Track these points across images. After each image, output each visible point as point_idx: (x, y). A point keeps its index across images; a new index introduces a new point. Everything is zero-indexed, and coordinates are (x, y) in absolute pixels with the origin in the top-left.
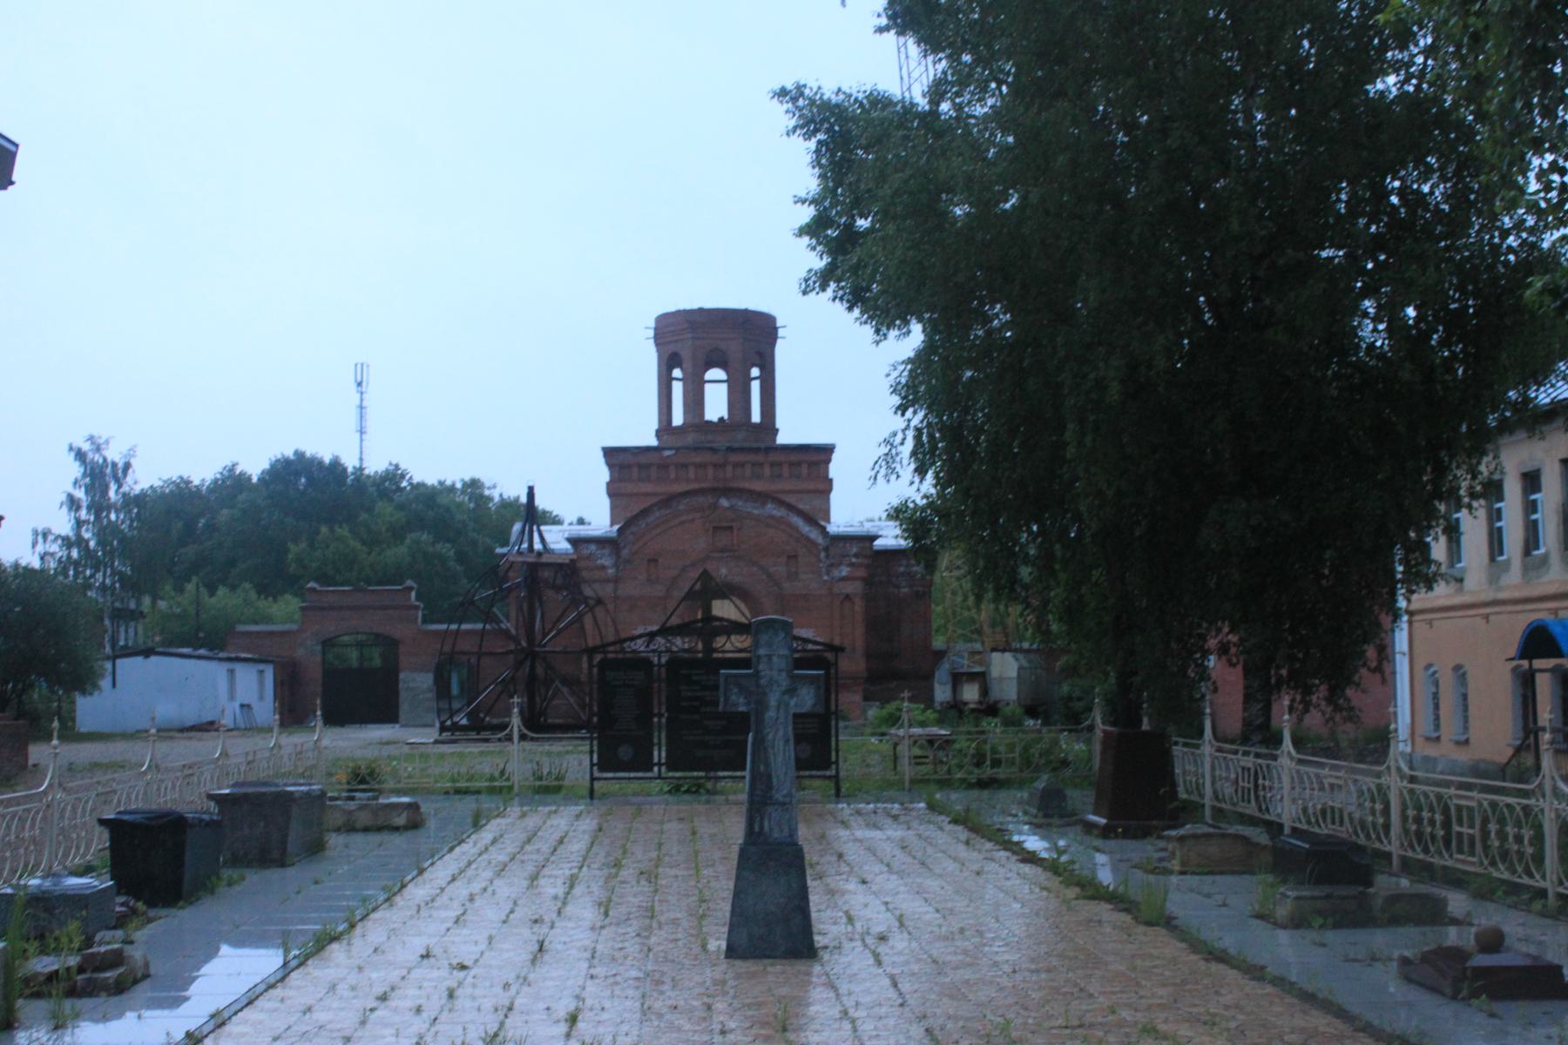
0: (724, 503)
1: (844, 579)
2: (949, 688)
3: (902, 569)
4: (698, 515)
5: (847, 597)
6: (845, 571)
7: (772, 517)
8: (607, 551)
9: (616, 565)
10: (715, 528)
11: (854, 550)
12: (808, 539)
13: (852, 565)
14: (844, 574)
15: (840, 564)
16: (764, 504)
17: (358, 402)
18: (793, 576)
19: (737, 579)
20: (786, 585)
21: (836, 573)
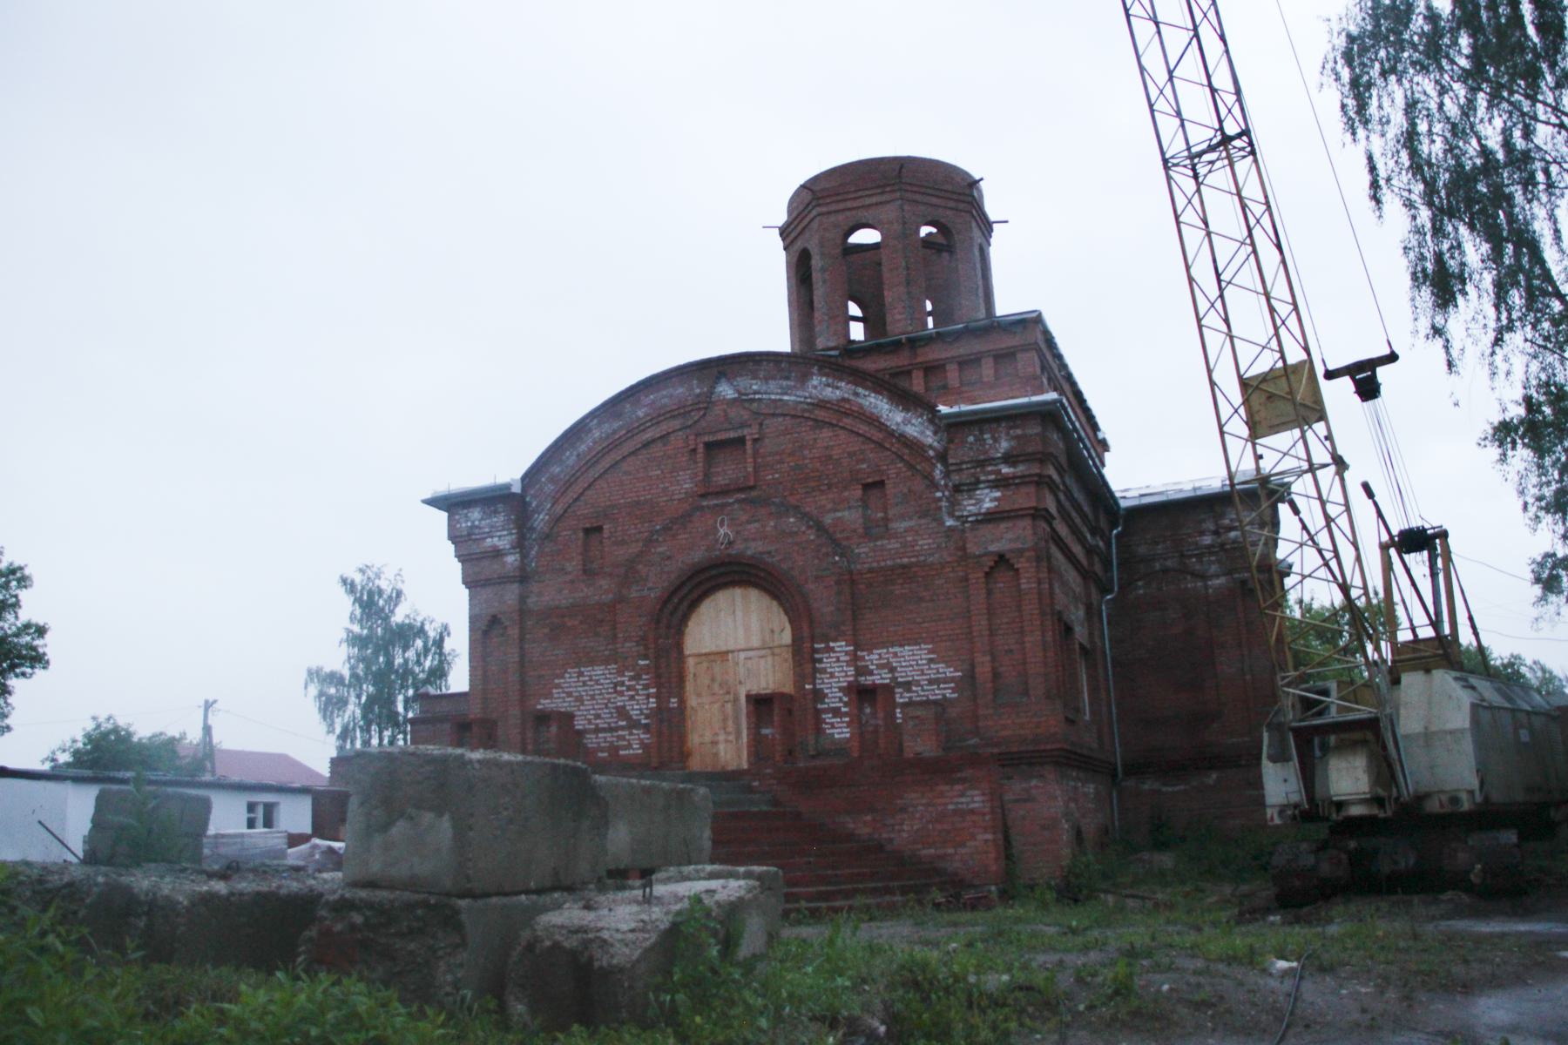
0: (726, 390)
1: (991, 517)
2: (1291, 770)
3: (1207, 540)
4: (676, 424)
5: (1001, 559)
6: (988, 500)
7: (822, 404)
8: (499, 519)
9: (520, 545)
10: (709, 446)
11: (1004, 445)
12: (903, 440)
13: (1001, 483)
14: (988, 505)
15: (975, 485)
16: (804, 378)
17: (1192, 271)
18: (874, 530)
19: (754, 548)
20: (863, 550)
21: (969, 507)
